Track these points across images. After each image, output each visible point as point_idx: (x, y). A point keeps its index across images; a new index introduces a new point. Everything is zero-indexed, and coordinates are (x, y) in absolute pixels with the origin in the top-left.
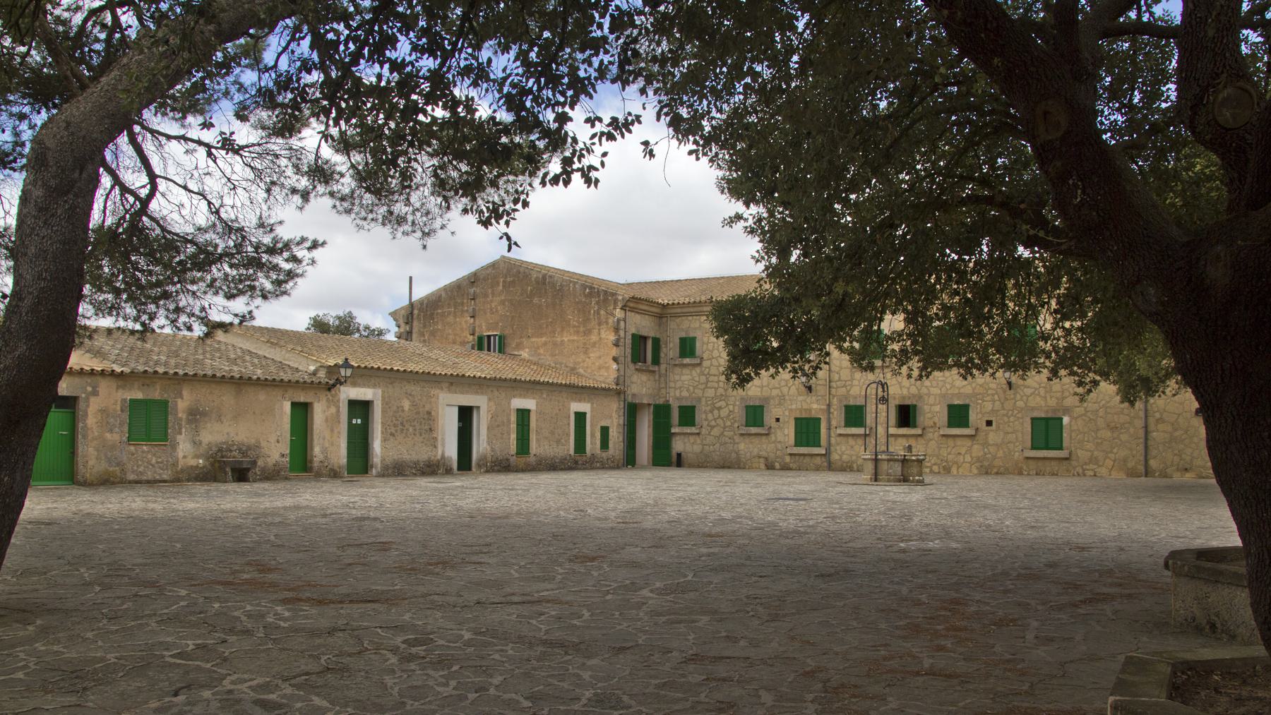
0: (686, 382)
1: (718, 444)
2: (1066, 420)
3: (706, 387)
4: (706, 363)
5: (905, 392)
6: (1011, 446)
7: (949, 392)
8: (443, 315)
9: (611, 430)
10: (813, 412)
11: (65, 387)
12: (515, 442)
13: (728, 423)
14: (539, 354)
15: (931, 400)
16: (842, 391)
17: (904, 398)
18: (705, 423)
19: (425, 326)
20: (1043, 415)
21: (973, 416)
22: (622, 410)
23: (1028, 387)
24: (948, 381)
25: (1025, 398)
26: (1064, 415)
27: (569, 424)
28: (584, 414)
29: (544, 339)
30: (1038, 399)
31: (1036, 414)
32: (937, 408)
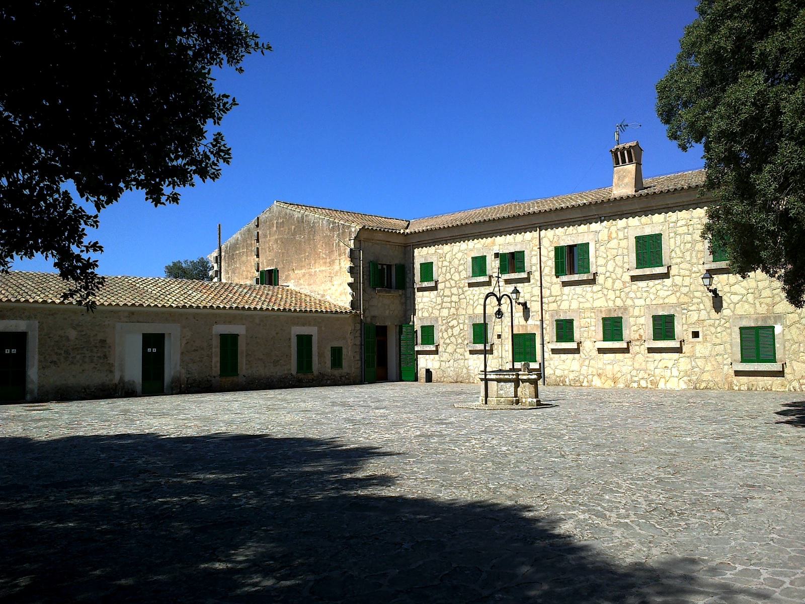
0: (427, 304)
1: (452, 361)
2: (778, 329)
3: (442, 308)
4: (440, 286)
5: (611, 304)
6: (719, 358)
7: (654, 302)
8: (240, 255)
9: (344, 351)
10: (529, 328)
11: (369, 320)
12: (219, 365)
13: (460, 341)
14: (301, 284)
15: (636, 312)
16: (553, 306)
17: (610, 310)
18: (441, 342)
19: (229, 265)
20: (753, 325)
21: (678, 328)
22: (359, 332)
23: (735, 294)
24: (651, 291)
25: (732, 306)
26: (776, 323)
27: (290, 346)
28: (309, 338)
29: (303, 271)
30: (746, 306)
31: (745, 323)
32: (642, 320)
